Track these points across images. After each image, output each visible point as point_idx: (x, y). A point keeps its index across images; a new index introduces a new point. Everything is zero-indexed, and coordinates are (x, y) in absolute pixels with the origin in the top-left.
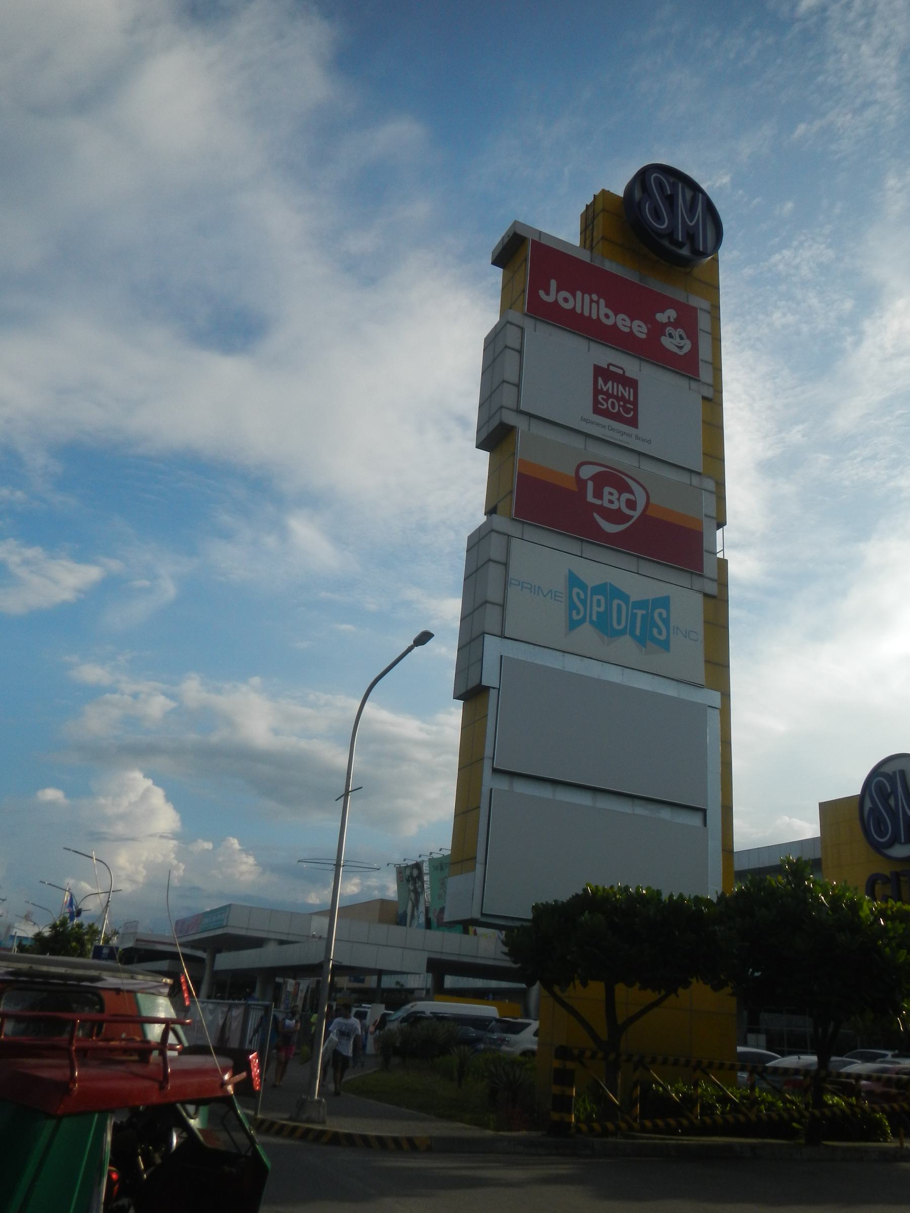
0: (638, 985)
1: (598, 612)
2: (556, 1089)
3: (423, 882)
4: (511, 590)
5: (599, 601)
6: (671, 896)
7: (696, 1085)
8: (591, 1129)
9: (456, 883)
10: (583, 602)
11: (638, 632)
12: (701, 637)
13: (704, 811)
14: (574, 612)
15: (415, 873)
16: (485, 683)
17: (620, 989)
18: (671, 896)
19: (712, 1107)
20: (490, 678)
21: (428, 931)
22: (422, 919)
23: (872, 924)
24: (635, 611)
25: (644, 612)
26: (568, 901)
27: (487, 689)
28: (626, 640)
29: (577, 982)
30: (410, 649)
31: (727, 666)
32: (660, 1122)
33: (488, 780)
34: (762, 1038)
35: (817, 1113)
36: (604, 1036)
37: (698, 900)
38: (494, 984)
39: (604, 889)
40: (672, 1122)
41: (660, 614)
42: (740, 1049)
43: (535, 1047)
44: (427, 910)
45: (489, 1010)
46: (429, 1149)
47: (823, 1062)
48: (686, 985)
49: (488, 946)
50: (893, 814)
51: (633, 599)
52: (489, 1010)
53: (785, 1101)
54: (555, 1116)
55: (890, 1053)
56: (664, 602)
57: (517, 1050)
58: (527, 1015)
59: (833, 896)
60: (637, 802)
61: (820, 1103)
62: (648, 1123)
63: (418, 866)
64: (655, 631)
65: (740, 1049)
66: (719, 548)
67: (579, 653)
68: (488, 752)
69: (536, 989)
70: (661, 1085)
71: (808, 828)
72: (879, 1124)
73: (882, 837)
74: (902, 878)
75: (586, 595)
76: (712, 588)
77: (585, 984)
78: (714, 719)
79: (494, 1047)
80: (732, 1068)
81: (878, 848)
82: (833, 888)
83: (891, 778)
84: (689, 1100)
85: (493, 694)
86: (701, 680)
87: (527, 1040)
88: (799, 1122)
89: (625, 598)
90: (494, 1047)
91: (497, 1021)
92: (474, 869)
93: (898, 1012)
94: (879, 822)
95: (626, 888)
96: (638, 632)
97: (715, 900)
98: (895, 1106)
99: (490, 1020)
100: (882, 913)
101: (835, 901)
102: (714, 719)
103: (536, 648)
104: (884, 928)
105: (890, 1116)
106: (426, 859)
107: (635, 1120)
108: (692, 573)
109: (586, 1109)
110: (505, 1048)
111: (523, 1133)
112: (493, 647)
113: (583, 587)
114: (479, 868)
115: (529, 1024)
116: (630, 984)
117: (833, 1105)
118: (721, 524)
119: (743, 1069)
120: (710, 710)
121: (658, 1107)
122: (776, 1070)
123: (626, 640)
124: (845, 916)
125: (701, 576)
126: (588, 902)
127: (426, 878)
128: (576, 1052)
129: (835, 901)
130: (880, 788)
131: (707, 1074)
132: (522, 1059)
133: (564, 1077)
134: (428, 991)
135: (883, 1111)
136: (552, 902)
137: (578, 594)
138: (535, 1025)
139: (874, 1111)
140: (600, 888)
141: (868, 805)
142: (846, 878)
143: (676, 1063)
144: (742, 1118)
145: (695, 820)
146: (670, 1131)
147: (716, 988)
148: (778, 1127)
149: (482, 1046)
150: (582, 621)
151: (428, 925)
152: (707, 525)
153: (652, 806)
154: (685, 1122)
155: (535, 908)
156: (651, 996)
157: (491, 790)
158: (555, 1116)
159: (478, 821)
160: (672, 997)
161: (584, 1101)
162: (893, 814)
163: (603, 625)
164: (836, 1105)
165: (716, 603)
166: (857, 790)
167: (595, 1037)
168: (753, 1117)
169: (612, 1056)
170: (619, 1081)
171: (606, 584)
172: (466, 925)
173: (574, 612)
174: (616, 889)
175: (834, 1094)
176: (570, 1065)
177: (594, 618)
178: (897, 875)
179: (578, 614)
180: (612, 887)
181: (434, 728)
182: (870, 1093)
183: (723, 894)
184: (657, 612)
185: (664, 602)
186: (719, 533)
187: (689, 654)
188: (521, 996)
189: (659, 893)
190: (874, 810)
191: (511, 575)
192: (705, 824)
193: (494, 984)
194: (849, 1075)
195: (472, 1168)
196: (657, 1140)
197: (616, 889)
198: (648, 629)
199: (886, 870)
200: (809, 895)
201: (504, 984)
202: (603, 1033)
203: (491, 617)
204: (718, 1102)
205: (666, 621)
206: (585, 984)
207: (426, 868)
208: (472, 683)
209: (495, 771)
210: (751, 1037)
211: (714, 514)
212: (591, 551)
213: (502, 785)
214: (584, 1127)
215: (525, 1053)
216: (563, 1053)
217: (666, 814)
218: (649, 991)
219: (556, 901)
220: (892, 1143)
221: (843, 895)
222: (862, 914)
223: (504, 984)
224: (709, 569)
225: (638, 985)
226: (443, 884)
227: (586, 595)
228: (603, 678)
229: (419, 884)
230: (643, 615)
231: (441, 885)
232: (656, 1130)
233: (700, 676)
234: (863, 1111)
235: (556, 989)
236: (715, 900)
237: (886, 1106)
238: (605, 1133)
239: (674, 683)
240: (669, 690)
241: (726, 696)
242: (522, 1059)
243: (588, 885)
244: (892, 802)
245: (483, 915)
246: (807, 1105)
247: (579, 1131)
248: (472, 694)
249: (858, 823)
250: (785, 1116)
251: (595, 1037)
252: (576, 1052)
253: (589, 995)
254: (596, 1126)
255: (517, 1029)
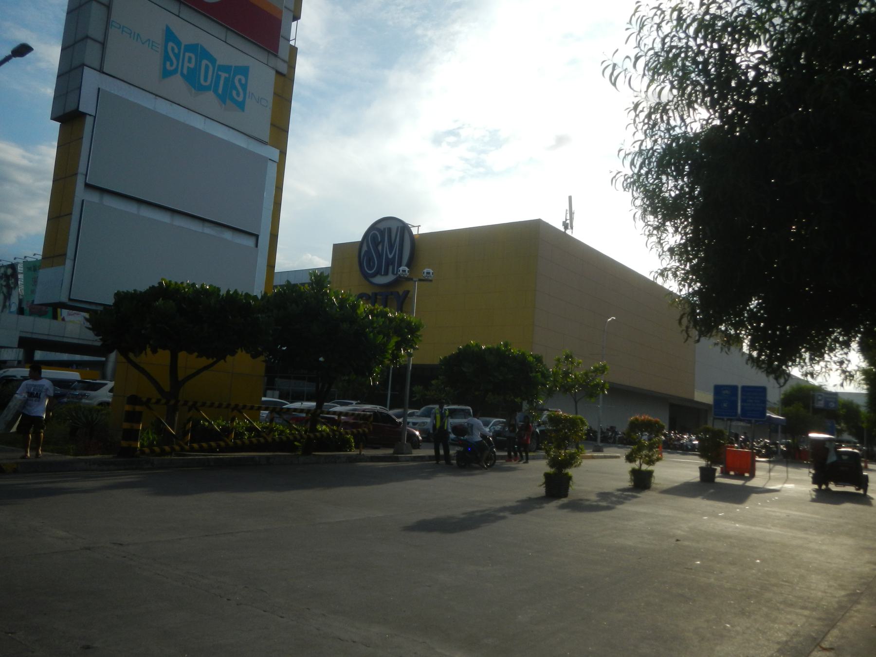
0: (196, 354)
1: (188, 68)
2: (126, 425)
3: (17, 280)
4: (113, 31)
5: (190, 58)
6: (228, 291)
7: (233, 420)
8: (153, 452)
9: (45, 275)
10: (177, 56)
11: (220, 91)
12: (270, 105)
13: (257, 236)
14: (168, 64)
15: (9, 271)
16: (81, 109)
17: (182, 355)
18: (228, 291)
19: (242, 434)
20: (87, 105)
21: (21, 317)
22: (14, 308)
23: (364, 318)
24: (220, 73)
25: (227, 75)
26: (145, 292)
27: (83, 115)
28: (210, 94)
29: (148, 350)
30: (7, 59)
31: (286, 131)
32: (204, 445)
33: (80, 192)
34: (277, 393)
35: (312, 435)
36: (167, 388)
37: (247, 295)
38: (78, 357)
39: (176, 283)
40: (213, 444)
41: (240, 80)
42: (264, 399)
43: (110, 400)
44: (20, 301)
45: (74, 375)
46: (15, 471)
47: (319, 406)
48: (233, 353)
49: (74, 326)
50: (380, 256)
51: (218, 63)
52: (74, 375)
53: (291, 429)
54: (124, 444)
55: (354, 402)
56: (244, 71)
57: (95, 402)
58: (104, 377)
59: (341, 299)
60: (207, 224)
61: (313, 429)
62: (195, 446)
63: (13, 266)
64: (234, 93)
65: (264, 399)
66: (292, 37)
67: (171, 99)
68: (82, 169)
69: (113, 356)
70: (207, 421)
71: (323, 261)
72: (348, 441)
73: (370, 270)
74: (378, 297)
75: (179, 49)
76: (283, 68)
77: (154, 351)
78: (272, 169)
79: (76, 400)
80: (259, 409)
81: (366, 276)
82: (342, 294)
83: (382, 232)
84: (226, 431)
85: (89, 121)
86: (267, 140)
87: (104, 394)
88: (299, 441)
89: (213, 61)
90: (76, 400)
91: (79, 381)
92: (64, 264)
93: (371, 374)
94: (370, 260)
95: (193, 285)
96: (220, 91)
97: (260, 297)
98: (360, 430)
99: (73, 381)
100: (371, 312)
101: (342, 302)
102: (272, 169)
103: (132, 87)
104: (372, 322)
105: (355, 436)
106: (21, 261)
107: (186, 444)
108: (269, 52)
109: (149, 439)
110: (84, 401)
111: (98, 456)
112: (91, 80)
113: (178, 43)
114: (69, 263)
115: (106, 384)
116: (190, 352)
117: (321, 431)
118: (297, 17)
119: (266, 409)
120: (270, 162)
121: (204, 435)
122: (288, 409)
123: (210, 94)
124: (348, 312)
125: (276, 56)
126: (163, 292)
127: (20, 276)
128: (144, 399)
129: (342, 302)
130: (374, 238)
131: (242, 413)
132: (99, 408)
133: (133, 417)
134: (19, 362)
135: (352, 434)
136: (131, 290)
137: (173, 49)
138: (111, 384)
139: (347, 434)
140: (173, 282)
141: (365, 248)
142: (348, 288)
143: (220, 406)
144: (262, 440)
145: (249, 242)
146: (211, 450)
147: (254, 357)
148: (286, 445)
149: (65, 400)
150: (175, 71)
151: (21, 311)
152: (286, 16)
153: (219, 229)
154: (222, 444)
155: (118, 295)
156: (204, 361)
157: (83, 201)
158: (124, 444)
159: (70, 223)
160: (222, 362)
161: (148, 433)
162: (380, 256)
163: (191, 78)
164: (324, 431)
165: (285, 79)
166: (359, 238)
167: (160, 389)
168: (270, 439)
169: (172, 402)
170: (176, 419)
171: (197, 45)
172: (53, 309)
173: (168, 64)
174: (185, 285)
175: (324, 424)
176: (138, 408)
177: (185, 72)
178: (376, 294)
179: (171, 65)
180: (182, 283)
181: (37, 157)
182: (346, 423)
183: (266, 293)
184: (238, 77)
185: (244, 71)
186: (294, 24)
187: (259, 117)
188: (102, 366)
189: (219, 290)
190: (368, 252)
191: (113, 18)
192: (257, 246)
193: (78, 357)
194: (334, 413)
195: (51, 482)
196: (201, 456)
197: (185, 285)
198: (229, 90)
199: (369, 291)
200: (325, 297)
201: (86, 358)
202: (166, 386)
203: (91, 53)
204: (246, 430)
205: (244, 87)
206: (154, 351)
207: (20, 269)
208: (71, 107)
209: (88, 186)
210: (269, 392)
211: (292, 8)
212: (186, 13)
213: (94, 198)
214: (147, 450)
215: (101, 404)
216: (133, 400)
217: (228, 235)
218: (204, 359)
219: (135, 290)
220: (354, 452)
221: (348, 299)
222: (359, 312)
223: (86, 358)
224: (283, 52)
225: (196, 354)
226: (35, 281)
227: (179, 49)
228: (187, 123)
229: (12, 281)
230: (225, 78)
231: (32, 282)
232: (202, 449)
233: (266, 135)
234: (341, 433)
235: (131, 355)
236: (260, 297)
237: (354, 430)
238: (163, 453)
239: (246, 137)
240: (241, 142)
241: (283, 153)
242: (99, 408)
243: (162, 279)
244: (380, 248)
245: (70, 300)
246: (306, 432)
247: (143, 452)
248: (69, 118)
249: (356, 260)
250: (291, 437)
251: (160, 389)
252: (144, 399)
253: (157, 360)
254: (157, 449)
255: (96, 387)
